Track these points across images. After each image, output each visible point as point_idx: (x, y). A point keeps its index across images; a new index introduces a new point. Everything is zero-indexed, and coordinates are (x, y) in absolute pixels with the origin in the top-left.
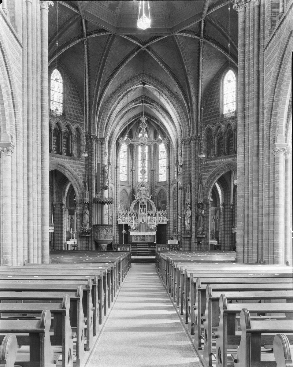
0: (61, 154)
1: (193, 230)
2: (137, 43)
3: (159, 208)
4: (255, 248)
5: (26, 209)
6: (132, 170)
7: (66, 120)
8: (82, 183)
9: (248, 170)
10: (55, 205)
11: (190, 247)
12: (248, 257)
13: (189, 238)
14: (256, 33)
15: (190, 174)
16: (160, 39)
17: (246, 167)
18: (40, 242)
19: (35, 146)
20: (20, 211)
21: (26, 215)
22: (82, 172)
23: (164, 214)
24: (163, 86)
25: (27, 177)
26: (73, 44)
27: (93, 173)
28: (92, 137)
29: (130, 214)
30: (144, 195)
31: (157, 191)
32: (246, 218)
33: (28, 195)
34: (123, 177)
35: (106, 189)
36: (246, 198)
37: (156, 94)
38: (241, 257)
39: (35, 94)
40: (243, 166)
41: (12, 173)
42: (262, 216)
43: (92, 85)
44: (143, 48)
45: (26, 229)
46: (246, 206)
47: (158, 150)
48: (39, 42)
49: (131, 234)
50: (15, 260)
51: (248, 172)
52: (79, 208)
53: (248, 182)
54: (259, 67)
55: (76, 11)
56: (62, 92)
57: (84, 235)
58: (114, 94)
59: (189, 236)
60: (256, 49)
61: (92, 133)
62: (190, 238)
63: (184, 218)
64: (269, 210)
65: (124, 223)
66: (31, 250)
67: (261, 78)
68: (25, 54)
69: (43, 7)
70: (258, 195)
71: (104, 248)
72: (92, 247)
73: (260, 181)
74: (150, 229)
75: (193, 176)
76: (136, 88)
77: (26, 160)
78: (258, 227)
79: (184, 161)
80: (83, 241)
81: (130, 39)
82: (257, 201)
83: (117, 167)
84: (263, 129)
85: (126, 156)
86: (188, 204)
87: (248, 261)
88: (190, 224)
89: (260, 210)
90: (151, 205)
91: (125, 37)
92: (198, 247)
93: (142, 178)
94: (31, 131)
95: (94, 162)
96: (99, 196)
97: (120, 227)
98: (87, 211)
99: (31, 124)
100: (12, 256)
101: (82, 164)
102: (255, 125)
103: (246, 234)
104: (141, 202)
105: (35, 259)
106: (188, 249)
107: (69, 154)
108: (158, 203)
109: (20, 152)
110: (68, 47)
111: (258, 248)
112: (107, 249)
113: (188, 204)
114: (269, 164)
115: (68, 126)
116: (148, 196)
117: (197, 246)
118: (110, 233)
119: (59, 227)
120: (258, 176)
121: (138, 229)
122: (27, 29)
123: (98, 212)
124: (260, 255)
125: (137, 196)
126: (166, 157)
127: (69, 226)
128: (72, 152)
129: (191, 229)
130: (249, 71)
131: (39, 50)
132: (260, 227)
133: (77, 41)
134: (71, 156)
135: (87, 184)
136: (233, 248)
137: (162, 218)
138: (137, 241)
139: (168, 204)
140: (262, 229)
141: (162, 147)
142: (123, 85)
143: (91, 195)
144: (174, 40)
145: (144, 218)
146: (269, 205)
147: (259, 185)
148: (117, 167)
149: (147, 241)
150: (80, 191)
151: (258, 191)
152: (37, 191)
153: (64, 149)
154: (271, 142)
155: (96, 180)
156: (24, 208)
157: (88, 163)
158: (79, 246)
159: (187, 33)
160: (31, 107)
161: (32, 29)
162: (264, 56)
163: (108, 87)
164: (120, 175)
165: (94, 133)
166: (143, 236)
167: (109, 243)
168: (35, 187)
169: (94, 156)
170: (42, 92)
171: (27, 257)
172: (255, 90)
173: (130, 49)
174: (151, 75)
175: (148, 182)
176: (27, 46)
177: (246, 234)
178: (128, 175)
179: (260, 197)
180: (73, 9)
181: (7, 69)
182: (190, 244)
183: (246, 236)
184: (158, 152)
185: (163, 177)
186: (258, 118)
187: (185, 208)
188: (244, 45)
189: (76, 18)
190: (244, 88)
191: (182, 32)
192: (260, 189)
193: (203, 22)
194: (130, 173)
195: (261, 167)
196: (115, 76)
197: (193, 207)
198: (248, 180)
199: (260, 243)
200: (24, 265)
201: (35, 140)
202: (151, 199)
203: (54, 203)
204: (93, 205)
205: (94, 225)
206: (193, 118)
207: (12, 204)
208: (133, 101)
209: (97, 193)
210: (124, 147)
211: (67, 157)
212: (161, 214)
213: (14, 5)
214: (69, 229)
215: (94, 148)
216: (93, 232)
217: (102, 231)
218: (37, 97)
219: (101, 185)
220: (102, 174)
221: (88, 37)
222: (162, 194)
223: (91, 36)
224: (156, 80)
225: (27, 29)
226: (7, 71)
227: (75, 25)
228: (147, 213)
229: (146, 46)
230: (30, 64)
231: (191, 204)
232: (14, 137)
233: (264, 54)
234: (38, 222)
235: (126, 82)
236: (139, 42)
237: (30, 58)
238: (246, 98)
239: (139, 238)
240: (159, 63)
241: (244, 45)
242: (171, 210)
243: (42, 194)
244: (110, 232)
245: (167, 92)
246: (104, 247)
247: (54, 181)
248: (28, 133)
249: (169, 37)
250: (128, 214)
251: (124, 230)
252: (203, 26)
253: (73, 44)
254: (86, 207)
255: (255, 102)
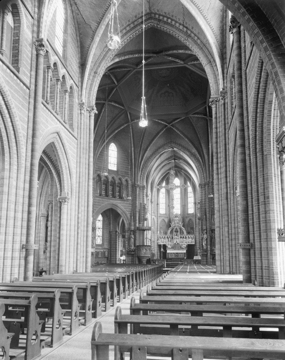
0: (115, 198)
1: (209, 249)
2: (165, 123)
3: (188, 233)
4: (228, 262)
5: (76, 237)
6: (169, 206)
7: (118, 175)
8: (129, 217)
9: (222, 209)
10: (112, 232)
11: (207, 262)
12: (224, 270)
13: (206, 255)
14: (223, 120)
15: (206, 209)
16: (180, 119)
17: (220, 207)
18: (85, 258)
19: (83, 197)
20: (72, 238)
21: (76, 241)
22: (129, 209)
23: (192, 237)
24: (186, 149)
25: (77, 217)
26: (122, 127)
27: (136, 210)
28: (136, 185)
29: (167, 237)
30: (178, 223)
31: (187, 220)
32: (221, 242)
33: (78, 228)
34: (162, 210)
35: (146, 220)
36: (221, 228)
37: (182, 153)
38: (219, 269)
39: (84, 167)
40: (218, 206)
41: (67, 215)
42: (232, 241)
43: (136, 152)
44: (169, 126)
45: (76, 250)
46: (221, 233)
47: (187, 191)
48: (88, 135)
49: (168, 251)
50: (67, 269)
51: (222, 210)
52: (127, 234)
53: (222, 217)
54: (225, 142)
55: (123, 108)
56: (116, 157)
57: (130, 253)
58: (151, 156)
59: (206, 253)
60: (223, 130)
61: (136, 182)
62: (207, 255)
63: (202, 240)
64: (235, 236)
65: (162, 244)
66: (79, 264)
67: (227, 148)
68: (79, 144)
69: (91, 115)
70: (228, 226)
71: (144, 262)
72: (135, 261)
73: (229, 216)
74: (181, 248)
75: (207, 210)
76: (168, 151)
77: (77, 207)
78: (229, 248)
79: (201, 200)
80: (130, 257)
81: (160, 121)
82: (228, 230)
83: (158, 204)
84: (230, 181)
85: (165, 196)
86: (205, 230)
87: (224, 272)
88: (207, 245)
89: (230, 236)
90: (183, 231)
91: (157, 120)
92: (213, 262)
93: (177, 210)
94: (81, 189)
95: (138, 202)
96: (141, 225)
97: (160, 246)
98: (133, 236)
99: (81, 184)
100: (65, 267)
101: (130, 204)
102: (225, 179)
103: (222, 253)
104: (175, 229)
105: (81, 269)
106: (205, 263)
107: (121, 197)
108: (188, 229)
109: (73, 202)
110: (119, 129)
111: (230, 263)
112: (147, 263)
113: (205, 230)
114: (234, 205)
115: (120, 179)
116: (181, 224)
117: (212, 261)
118: (148, 251)
119: (114, 247)
120: (228, 213)
121: (173, 248)
122: (81, 129)
123: (140, 236)
124: (231, 268)
125: (173, 225)
126: (193, 196)
127: (122, 246)
128: (122, 195)
129: (207, 248)
130: (220, 144)
131: (88, 140)
132: (230, 248)
133: (125, 125)
134: (122, 198)
135: (132, 217)
136: (214, 263)
137: (190, 240)
138: (172, 257)
139: (195, 229)
140: (232, 249)
141: (190, 189)
142: (157, 150)
143: (135, 225)
144: (189, 120)
145: (177, 240)
146: (235, 233)
147: (228, 219)
148: (158, 204)
149: (179, 257)
150: (128, 222)
151: (228, 223)
152: (84, 225)
153: (117, 194)
154: (235, 190)
155: (139, 214)
156: (74, 236)
157: (134, 203)
158: (127, 260)
159: (198, 114)
160: (81, 174)
161: (84, 129)
162: (228, 134)
163: (147, 152)
164: (160, 209)
165: (137, 182)
166: (177, 253)
167: (147, 258)
168: (83, 223)
169: (138, 198)
170: (89, 165)
171: (76, 268)
172: (224, 156)
173: (160, 128)
174: (177, 142)
175: (181, 214)
176: (80, 138)
177: (222, 253)
178: (166, 209)
179: (230, 227)
180: (121, 107)
181: (66, 154)
182: (207, 259)
183: (222, 254)
184: (187, 193)
185: (191, 210)
186: (226, 174)
187: (202, 233)
188: (216, 128)
189: (123, 111)
190: (217, 155)
191: (194, 114)
192: (230, 221)
193: (207, 107)
194: (167, 208)
195: (229, 207)
196: (152, 145)
197: (208, 232)
198: (222, 215)
199: (231, 259)
200: (73, 273)
201: (83, 194)
202: (183, 226)
203: (111, 230)
204: (136, 231)
205: (137, 246)
206: (206, 169)
207: (66, 234)
208: (166, 159)
209: (139, 223)
210: (163, 191)
211: (119, 199)
212: (190, 237)
213: (73, 116)
214: (122, 248)
215: (138, 193)
216: (136, 251)
217: (143, 250)
218: (86, 168)
219: (142, 218)
220: (143, 210)
221: (132, 122)
222: (191, 222)
223: (134, 122)
224: (180, 145)
225: (81, 129)
226: (66, 155)
227: (123, 116)
228: (180, 237)
229: (171, 124)
230: (82, 149)
231: (206, 230)
232: (70, 193)
233: (228, 133)
234: (83, 245)
235: (159, 148)
236: (166, 123)
237: (82, 146)
238: (219, 162)
239: (174, 255)
240: (181, 135)
241: (216, 128)
242: (197, 234)
243: (87, 227)
244: (148, 251)
245: (188, 153)
246: (144, 261)
247: (111, 216)
248: (79, 190)
249: (186, 118)
250: (166, 237)
251: (162, 249)
252: (208, 109)
253: (122, 127)
254: (132, 233)
255: (224, 164)
